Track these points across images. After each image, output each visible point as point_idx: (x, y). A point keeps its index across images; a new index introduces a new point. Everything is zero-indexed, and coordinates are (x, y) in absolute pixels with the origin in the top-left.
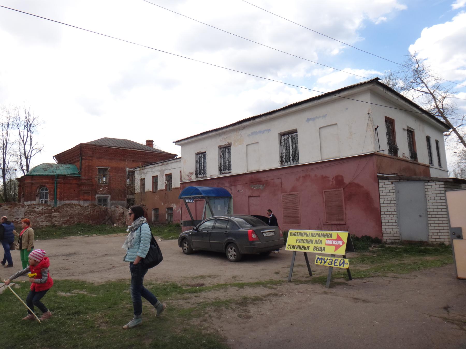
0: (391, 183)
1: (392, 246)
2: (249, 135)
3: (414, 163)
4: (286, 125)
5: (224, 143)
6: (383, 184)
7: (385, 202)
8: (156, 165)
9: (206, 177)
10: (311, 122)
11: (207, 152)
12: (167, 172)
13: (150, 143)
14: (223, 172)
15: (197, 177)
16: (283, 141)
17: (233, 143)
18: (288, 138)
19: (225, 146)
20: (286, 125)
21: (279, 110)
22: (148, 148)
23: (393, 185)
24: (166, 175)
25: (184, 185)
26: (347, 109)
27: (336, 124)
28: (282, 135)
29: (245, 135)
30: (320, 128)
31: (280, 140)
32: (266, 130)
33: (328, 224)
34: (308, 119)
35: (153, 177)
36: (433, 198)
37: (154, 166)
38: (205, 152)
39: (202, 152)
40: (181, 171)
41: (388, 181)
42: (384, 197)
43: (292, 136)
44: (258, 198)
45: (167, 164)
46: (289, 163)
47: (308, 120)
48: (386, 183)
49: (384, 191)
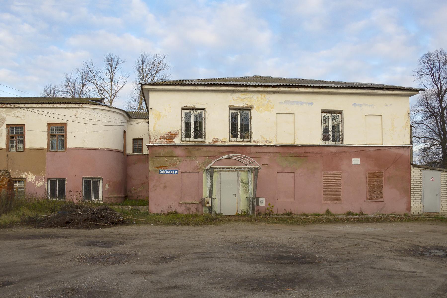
17: (255, 107)
20: (239, 100)
24: (8, 125)
27: (381, 115)
28: (323, 112)
33: (369, 201)
39: (196, 107)
47: (354, 104)
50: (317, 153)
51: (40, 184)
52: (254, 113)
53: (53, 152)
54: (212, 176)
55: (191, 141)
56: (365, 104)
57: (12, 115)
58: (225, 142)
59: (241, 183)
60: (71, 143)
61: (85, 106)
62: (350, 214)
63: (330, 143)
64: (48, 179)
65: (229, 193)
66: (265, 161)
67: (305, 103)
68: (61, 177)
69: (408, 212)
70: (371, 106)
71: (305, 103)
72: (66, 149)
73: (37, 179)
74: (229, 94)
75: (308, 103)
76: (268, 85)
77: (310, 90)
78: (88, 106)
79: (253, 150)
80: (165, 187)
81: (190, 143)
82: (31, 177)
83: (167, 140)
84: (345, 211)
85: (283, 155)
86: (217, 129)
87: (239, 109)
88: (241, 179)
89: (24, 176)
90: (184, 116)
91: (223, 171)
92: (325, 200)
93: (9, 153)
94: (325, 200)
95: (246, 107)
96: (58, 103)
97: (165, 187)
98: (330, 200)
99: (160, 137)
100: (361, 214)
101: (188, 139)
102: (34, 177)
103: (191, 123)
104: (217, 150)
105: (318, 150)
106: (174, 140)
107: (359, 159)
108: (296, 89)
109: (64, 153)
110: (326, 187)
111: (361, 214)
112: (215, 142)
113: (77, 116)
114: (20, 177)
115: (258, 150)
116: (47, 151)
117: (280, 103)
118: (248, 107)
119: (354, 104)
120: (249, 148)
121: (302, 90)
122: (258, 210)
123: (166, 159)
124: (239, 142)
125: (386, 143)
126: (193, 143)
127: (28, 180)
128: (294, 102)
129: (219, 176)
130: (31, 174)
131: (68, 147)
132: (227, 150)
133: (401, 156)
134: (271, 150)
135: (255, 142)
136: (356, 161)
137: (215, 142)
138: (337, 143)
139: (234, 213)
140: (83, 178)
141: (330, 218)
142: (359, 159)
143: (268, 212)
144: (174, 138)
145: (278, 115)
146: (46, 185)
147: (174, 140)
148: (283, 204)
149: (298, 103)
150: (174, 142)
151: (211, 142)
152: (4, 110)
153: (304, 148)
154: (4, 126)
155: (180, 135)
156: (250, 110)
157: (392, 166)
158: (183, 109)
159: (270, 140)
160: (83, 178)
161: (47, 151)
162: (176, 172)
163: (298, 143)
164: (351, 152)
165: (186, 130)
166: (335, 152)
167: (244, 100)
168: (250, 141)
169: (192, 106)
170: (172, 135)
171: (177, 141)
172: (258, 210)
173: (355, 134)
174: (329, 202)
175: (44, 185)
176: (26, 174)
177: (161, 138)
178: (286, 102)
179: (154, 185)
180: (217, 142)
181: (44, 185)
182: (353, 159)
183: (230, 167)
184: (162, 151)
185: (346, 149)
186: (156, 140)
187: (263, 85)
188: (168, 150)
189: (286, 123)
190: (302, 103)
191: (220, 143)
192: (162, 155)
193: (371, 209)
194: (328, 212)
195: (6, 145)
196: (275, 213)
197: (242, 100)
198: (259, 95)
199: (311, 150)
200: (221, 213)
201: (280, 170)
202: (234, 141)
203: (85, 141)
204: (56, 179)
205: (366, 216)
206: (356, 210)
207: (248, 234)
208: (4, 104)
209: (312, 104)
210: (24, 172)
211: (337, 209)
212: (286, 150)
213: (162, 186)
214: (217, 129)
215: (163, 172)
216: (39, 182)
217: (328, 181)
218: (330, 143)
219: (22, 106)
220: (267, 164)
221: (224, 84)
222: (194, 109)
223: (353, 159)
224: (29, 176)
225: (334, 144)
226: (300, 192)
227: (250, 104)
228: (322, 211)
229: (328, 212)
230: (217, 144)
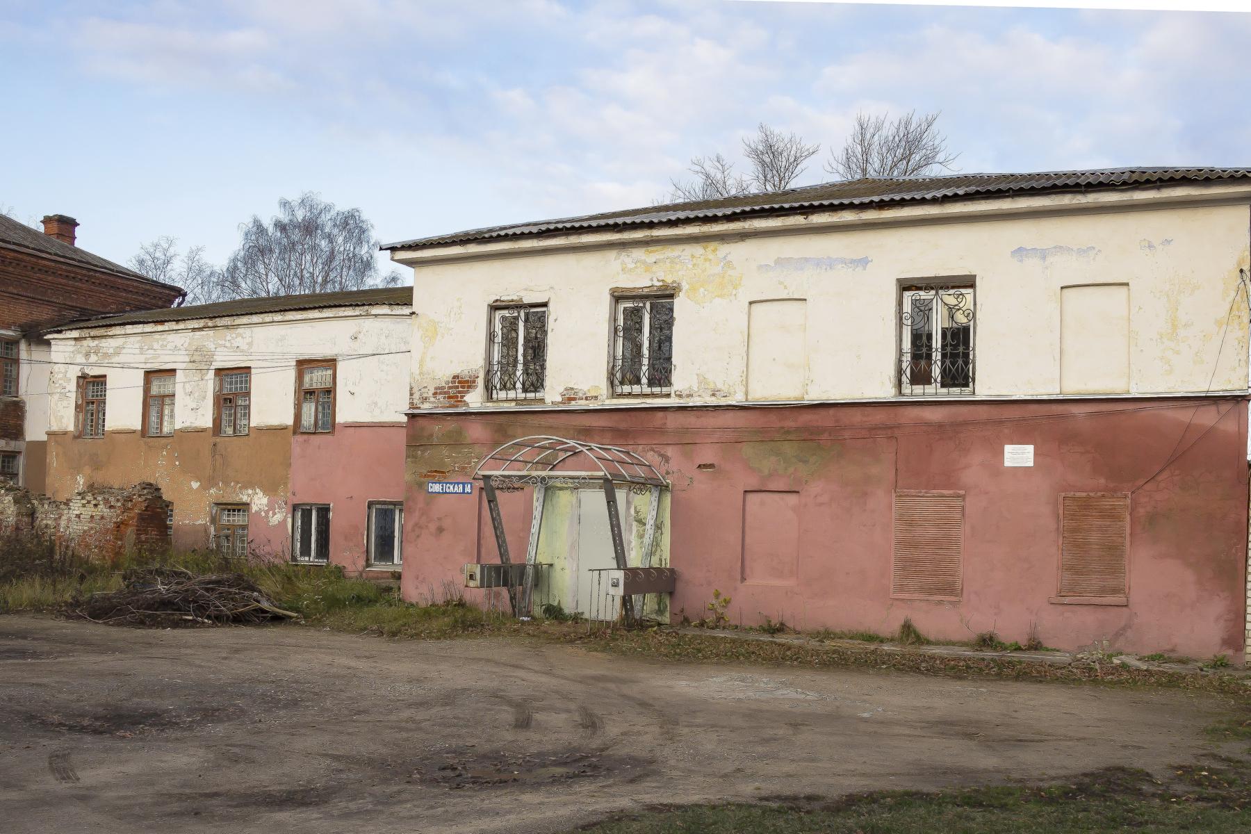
1: (421, 715)
8: (173, 325)
9: (542, 400)
11: (551, 305)
12: (226, 359)
13: (64, 226)
14: (619, 390)
15: (490, 398)
16: (907, 307)
17: (685, 286)
18: (516, 318)
19: (640, 292)
20: (638, 269)
22: (56, 245)
24: (219, 371)
25: (421, 422)
26: (1168, 242)
27: (1127, 284)
28: (905, 286)
29: (756, 262)
30: (751, 303)
31: (900, 304)
33: (1066, 600)
35: (150, 375)
37: (160, 328)
38: (545, 305)
39: (526, 301)
43: (527, 315)
44: (792, 499)
45: (227, 327)
47: (1020, 252)
50: (874, 429)
51: (276, 519)
52: (679, 304)
53: (306, 437)
54: (611, 501)
55: (507, 400)
56: (1059, 249)
57: (228, 344)
58: (596, 397)
59: (635, 524)
60: (346, 412)
61: (376, 310)
62: (986, 641)
63: (934, 391)
64: (295, 508)
65: (581, 549)
66: (708, 455)
67: (844, 261)
68: (322, 501)
69: (1230, 652)
70: (1082, 252)
71: (844, 261)
72: (334, 425)
73: (271, 507)
74: (612, 255)
75: (852, 261)
76: (634, 223)
77: (848, 217)
78: (385, 310)
79: (672, 421)
80: (440, 530)
81: (506, 405)
82: (259, 501)
83: (449, 397)
84: (971, 635)
85: (763, 437)
86: (579, 363)
87: (646, 297)
88: (637, 512)
89: (245, 499)
90: (907, 307)
91: (588, 486)
92: (901, 588)
93: (218, 440)
94: (901, 588)
95: (659, 288)
96: (315, 308)
97: (440, 530)
98: (921, 590)
99: (433, 391)
100: (1035, 646)
101: (918, 389)
102: (265, 501)
103: (929, 336)
104: (580, 421)
105: (880, 416)
106: (467, 398)
107: (1030, 448)
108: (799, 220)
109: (329, 437)
110: (905, 544)
111: (1035, 646)
112: (570, 399)
113: (360, 336)
114: (237, 500)
115: (690, 420)
116: (295, 433)
117: (760, 267)
118: (666, 287)
119: (1020, 252)
120: (660, 414)
121: (657, 233)
122: (682, 611)
123: (445, 452)
124: (640, 396)
125: (1138, 389)
126: (513, 404)
127: (254, 508)
128: (807, 260)
129: (574, 500)
130: (261, 494)
131: (338, 420)
132: (603, 424)
133: (1209, 433)
134: (728, 419)
135: (680, 396)
136: (1019, 455)
137: (570, 399)
138: (955, 393)
139: (440, 600)
140: (370, 505)
141: (909, 656)
142: (1030, 448)
143: (710, 618)
144: (467, 392)
145: (1065, 291)
146: (290, 520)
147: (467, 398)
148: (763, 593)
149: (818, 263)
150: (466, 404)
151: (559, 399)
152: (211, 333)
153: (832, 411)
154: (212, 373)
155: (480, 382)
156: (672, 296)
157: (1165, 475)
158: (494, 308)
159: (725, 389)
160: (370, 505)
161: (295, 433)
162: (468, 489)
163: (815, 395)
164: (1001, 422)
165: (916, 357)
166: (940, 426)
167: (654, 268)
168: (668, 395)
169: (515, 298)
170: (463, 384)
171: (475, 400)
172: (682, 611)
173: (706, 364)
174: (916, 596)
175: (285, 520)
176: (250, 492)
177: (435, 394)
178: (779, 262)
179: (416, 525)
180: (574, 399)
181: (285, 520)
182: (1008, 448)
183: (589, 473)
184: (437, 428)
185: (983, 412)
186: (425, 399)
187: (701, 215)
188: (451, 425)
189: (799, 330)
190: (830, 263)
191: (583, 402)
192: (435, 441)
193: (1070, 631)
194: (908, 631)
195: (214, 421)
196: (733, 623)
197: (648, 268)
198: (697, 249)
199: (857, 417)
200: (580, 610)
201: (753, 483)
202: (630, 395)
203: (376, 404)
204: (311, 505)
205: (1049, 658)
206: (1011, 628)
207: (790, 693)
208: (211, 318)
209: (864, 262)
210: (245, 487)
211: (943, 623)
212: (773, 420)
213: (433, 527)
214: (579, 363)
215: (437, 488)
216: (274, 514)
217: (911, 523)
218: (934, 391)
219: (245, 320)
220: (711, 466)
221: (913, 199)
222: (519, 306)
223: (1008, 448)
224: (256, 497)
225: (945, 394)
226: (815, 555)
227: (669, 280)
228: (887, 621)
229: (908, 631)
230: (574, 406)
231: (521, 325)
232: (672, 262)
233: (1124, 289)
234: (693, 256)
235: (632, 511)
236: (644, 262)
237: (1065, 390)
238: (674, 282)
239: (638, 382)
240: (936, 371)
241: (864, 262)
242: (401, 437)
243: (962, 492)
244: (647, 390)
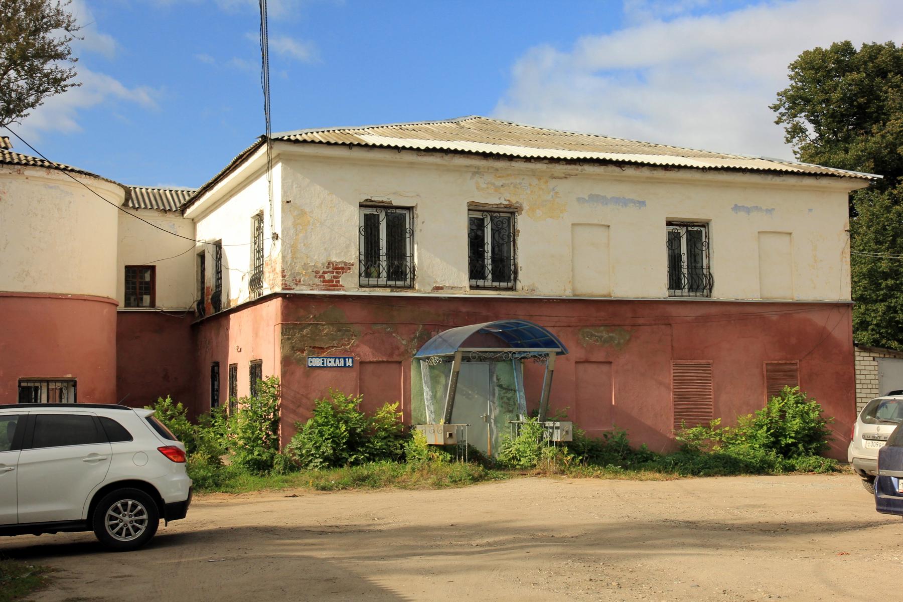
0: (871, 359)
2: (579, 200)
3: (388, 362)
4: (689, 205)
5: (492, 199)
6: (861, 358)
7: (863, 391)
10: (742, 214)
17: (526, 207)
21: (33, 463)
23: (875, 363)
26: (810, 210)
30: (573, 225)
32: (633, 201)
34: (736, 205)
36: (865, 386)
39: (395, 204)
40: (260, 217)
41: (867, 354)
42: (863, 382)
44: (605, 368)
46: (678, 292)
47: (736, 208)
48: (865, 359)
49: (863, 372)
56: (757, 208)
59: (497, 389)
117: (579, 199)
162: (349, 363)
169: (385, 199)
171: (350, 285)
197: (497, 189)
215: (317, 362)
227: (514, 201)
231: (684, 241)
232: (515, 187)
233: (787, 238)
234: (530, 185)
235: (495, 379)
236: (493, 184)
237: (578, 293)
238: (517, 202)
239: (484, 277)
240: (685, 281)
241: (642, 203)
242: (108, 316)
243: (711, 361)
244: (488, 283)
